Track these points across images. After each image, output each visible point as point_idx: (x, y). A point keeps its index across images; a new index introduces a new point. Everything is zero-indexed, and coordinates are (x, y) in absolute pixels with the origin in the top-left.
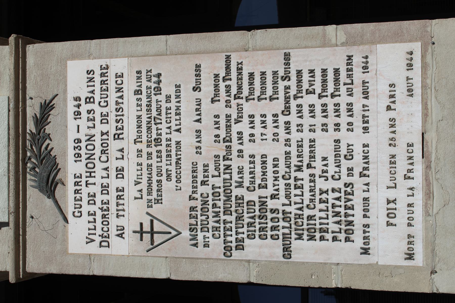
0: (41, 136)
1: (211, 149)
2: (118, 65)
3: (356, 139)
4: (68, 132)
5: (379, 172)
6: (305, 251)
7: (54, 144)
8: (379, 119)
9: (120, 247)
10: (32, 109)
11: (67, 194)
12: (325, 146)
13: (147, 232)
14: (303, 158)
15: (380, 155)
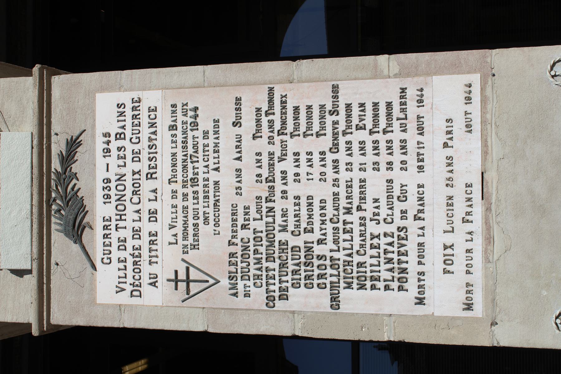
0: (67, 176)
1: (253, 190)
2: (151, 98)
3: (410, 179)
4: (96, 172)
5: (435, 215)
6: (354, 301)
7: (82, 185)
8: (435, 157)
9: (153, 297)
10: (58, 146)
11: (95, 239)
12: (376, 187)
13: (182, 281)
14: (352, 200)
15: (436, 197)
